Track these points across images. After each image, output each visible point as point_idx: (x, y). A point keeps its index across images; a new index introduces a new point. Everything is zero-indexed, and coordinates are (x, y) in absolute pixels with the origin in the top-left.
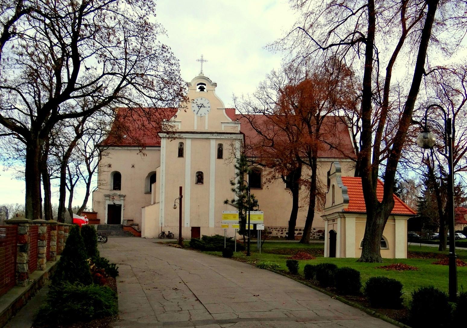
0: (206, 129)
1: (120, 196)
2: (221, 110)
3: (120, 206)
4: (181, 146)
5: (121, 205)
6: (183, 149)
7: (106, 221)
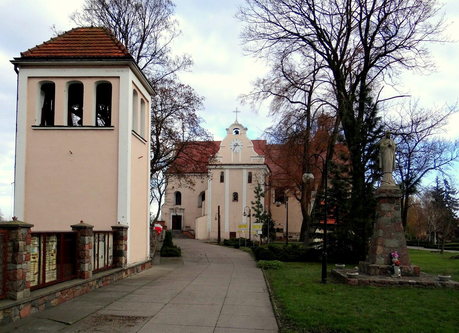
0: (240, 161)
2: (250, 148)
3: (180, 217)
4: (222, 174)
6: (223, 176)
7: (171, 228)
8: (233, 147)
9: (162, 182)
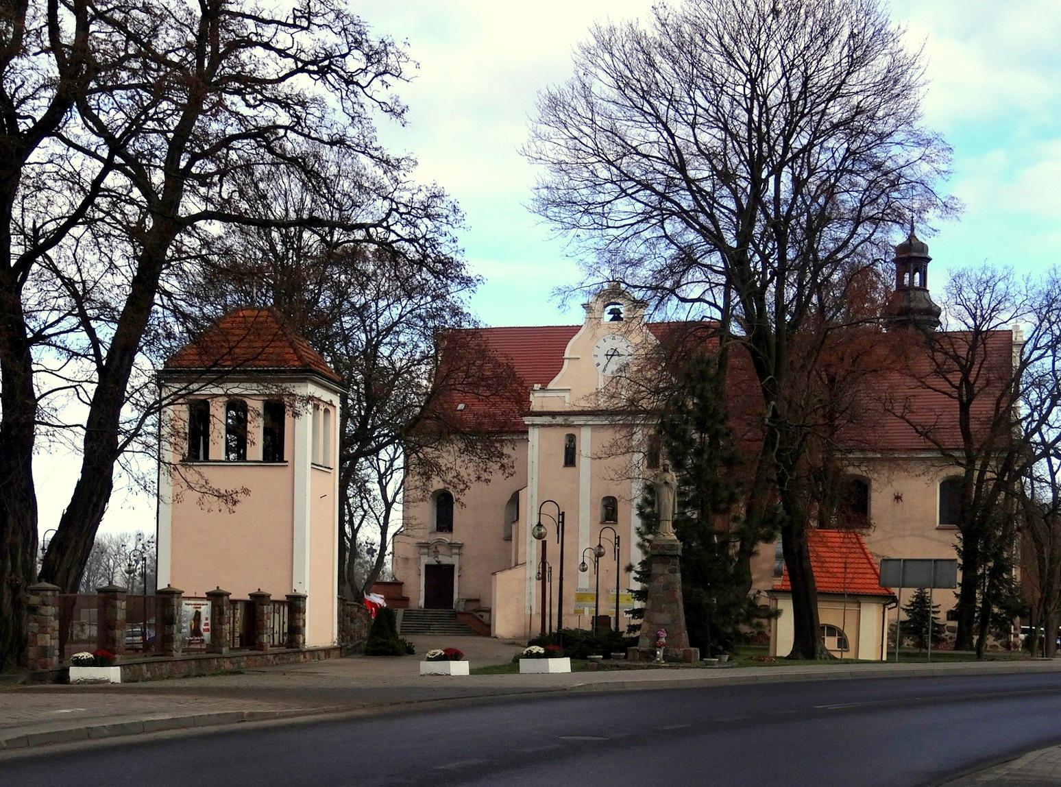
1: (452, 545)
3: (451, 568)
5: (452, 567)
6: (574, 448)
7: (422, 602)
8: (604, 361)
9: (391, 465)
